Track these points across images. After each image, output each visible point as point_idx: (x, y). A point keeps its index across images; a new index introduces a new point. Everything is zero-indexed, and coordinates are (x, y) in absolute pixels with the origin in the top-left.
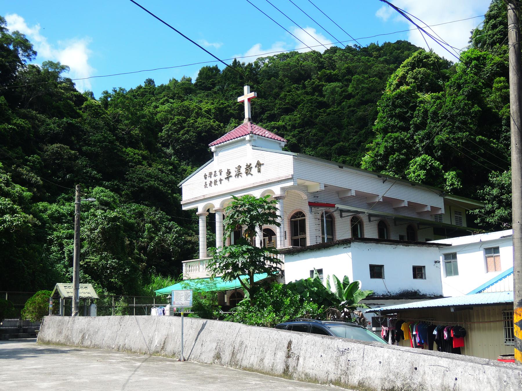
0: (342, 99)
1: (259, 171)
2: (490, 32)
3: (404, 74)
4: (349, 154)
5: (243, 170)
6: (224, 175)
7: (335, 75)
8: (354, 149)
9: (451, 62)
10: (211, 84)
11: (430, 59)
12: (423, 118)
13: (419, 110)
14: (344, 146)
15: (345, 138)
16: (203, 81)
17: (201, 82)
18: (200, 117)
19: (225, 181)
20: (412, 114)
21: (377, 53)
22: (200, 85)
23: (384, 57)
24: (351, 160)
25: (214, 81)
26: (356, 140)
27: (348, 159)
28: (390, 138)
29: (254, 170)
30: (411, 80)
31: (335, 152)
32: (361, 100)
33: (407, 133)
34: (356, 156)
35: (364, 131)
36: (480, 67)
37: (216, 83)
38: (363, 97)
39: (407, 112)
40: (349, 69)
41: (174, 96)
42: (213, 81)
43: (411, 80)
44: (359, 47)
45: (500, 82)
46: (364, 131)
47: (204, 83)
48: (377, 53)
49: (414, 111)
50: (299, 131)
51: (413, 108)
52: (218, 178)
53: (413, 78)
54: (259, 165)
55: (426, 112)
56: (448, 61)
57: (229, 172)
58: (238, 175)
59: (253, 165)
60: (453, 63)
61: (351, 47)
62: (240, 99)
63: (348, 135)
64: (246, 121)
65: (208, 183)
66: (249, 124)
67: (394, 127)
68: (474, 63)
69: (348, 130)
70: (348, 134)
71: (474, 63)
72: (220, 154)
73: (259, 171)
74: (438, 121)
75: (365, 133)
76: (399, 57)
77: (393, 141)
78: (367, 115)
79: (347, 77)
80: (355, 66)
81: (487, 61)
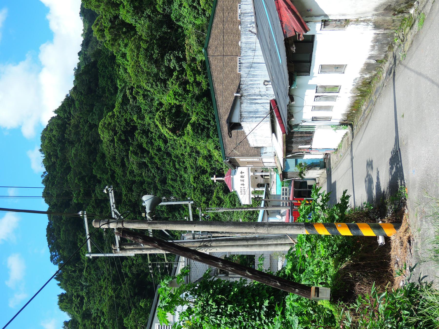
0: (114, 183)
1: (243, 173)
2: (159, 88)
3: (168, 129)
4: (166, 176)
5: (242, 179)
6: (243, 186)
7: (84, 190)
8: (162, 173)
9: (67, 96)
10: (78, 299)
11: (161, 115)
12: (205, 121)
13: (202, 122)
14: (159, 179)
15: (152, 179)
16: (74, 305)
17: (74, 308)
18: (120, 295)
19: (245, 186)
20: (202, 125)
21: (53, 158)
22: (78, 308)
23: (58, 151)
24: (171, 175)
25: (75, 296)
26: (156, 171)
27: (170, 177)
28: (212, 135)
29: (243, 174)
30: (171, 126)
31: (163, 186)
32: (121, 167)
33: (210, 128)
34: (168, 171)
35: (149, 165)
36: (179, 94)
37: (77, 294)
38: (118, 165)
39: (201, 127)
40: (80, 178)
41: (93, 323)
42: (75, 297)
43: (171, 126)
44: (44, 173)
45: (189, 87)
46: (149, 165)
47: (76, 305)
48: (53, 158)
49: (201, 124)
50: (139, 216)
51: (200, 124)
52: (243, 189)
53: (171, 124)
54: (241, 173)
55: (203, 119)
56: (66, 98)
57: (242, 184)
58: (243, 181)
59: (241, 175)
60: (68, 95)
61: (43, 180)
62: (215, 181)
63: (150, 176)
64: (223, 179)
65: (244, 193)
66: (225, 178)
67: (207, 133)
68: (177, 97)
69: (146, 177)
70: (149, 177)
71: (177, 97)
72: (235, 188)
73: (243, 173)
74: (208, 115)
75: (151, 164)
76: (58, 139)
77: (214, 134)
78: (137, 162)
79: (87, 181)
80: (74, 175)
81: (177, 91)
